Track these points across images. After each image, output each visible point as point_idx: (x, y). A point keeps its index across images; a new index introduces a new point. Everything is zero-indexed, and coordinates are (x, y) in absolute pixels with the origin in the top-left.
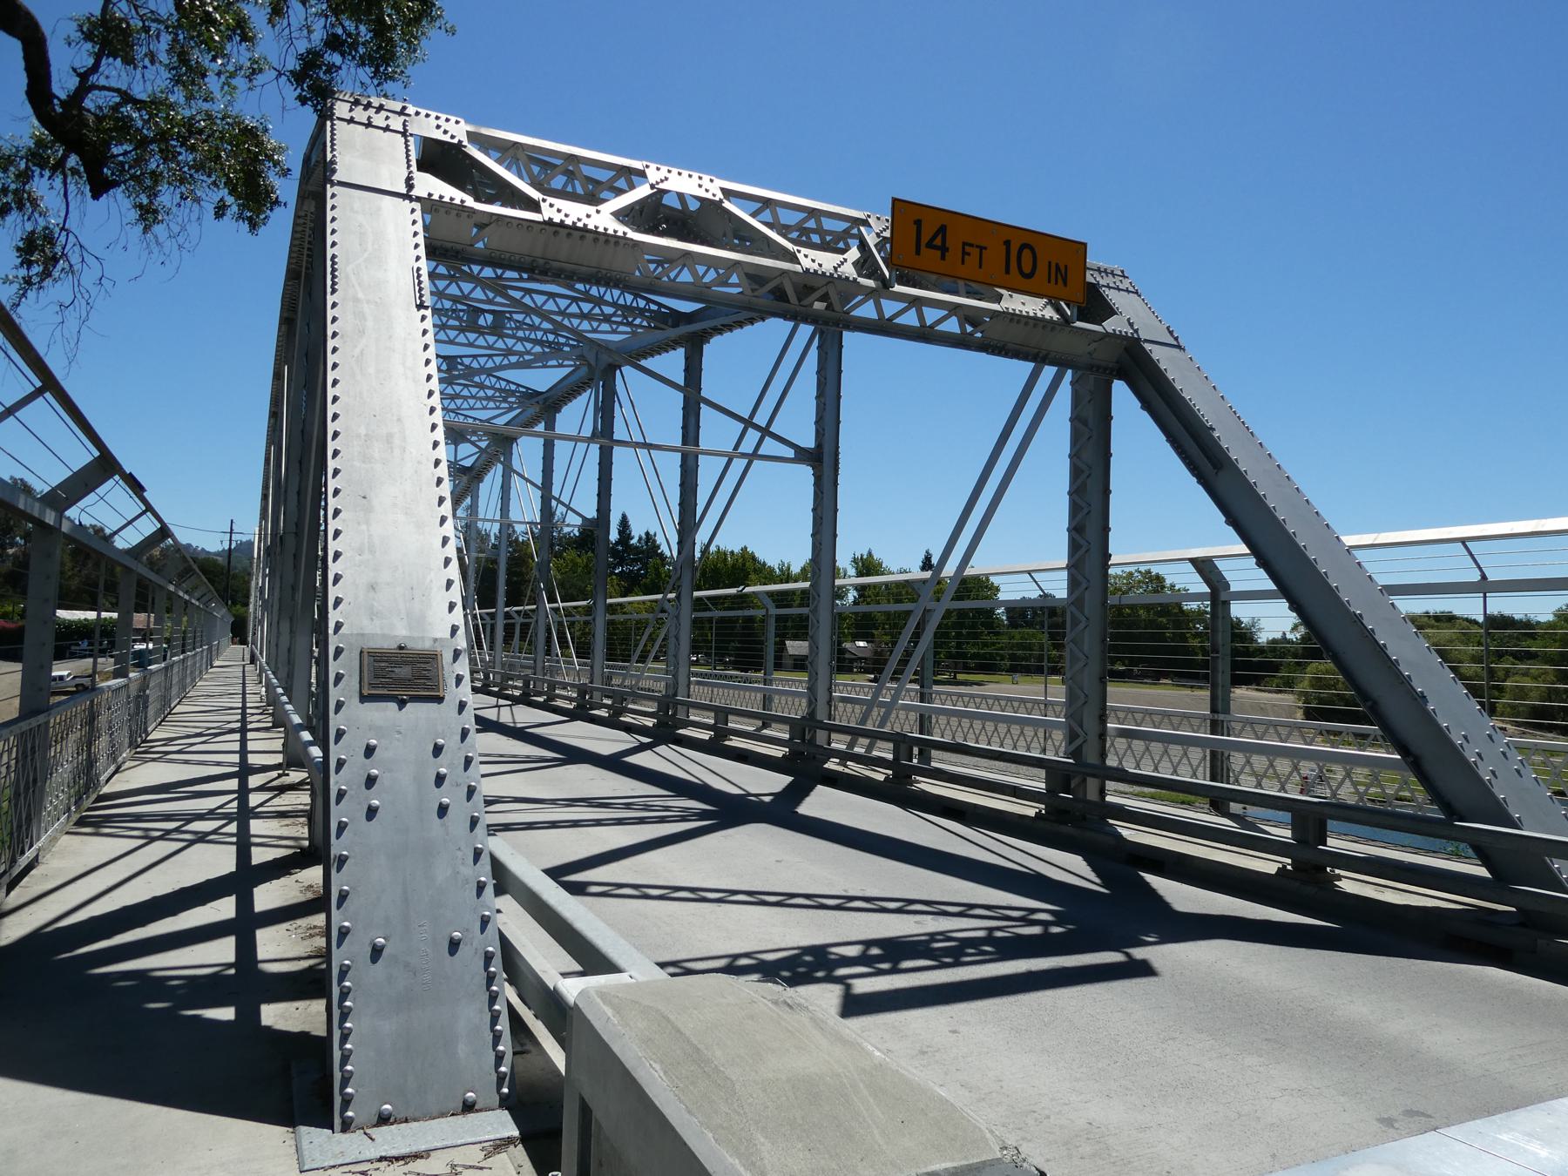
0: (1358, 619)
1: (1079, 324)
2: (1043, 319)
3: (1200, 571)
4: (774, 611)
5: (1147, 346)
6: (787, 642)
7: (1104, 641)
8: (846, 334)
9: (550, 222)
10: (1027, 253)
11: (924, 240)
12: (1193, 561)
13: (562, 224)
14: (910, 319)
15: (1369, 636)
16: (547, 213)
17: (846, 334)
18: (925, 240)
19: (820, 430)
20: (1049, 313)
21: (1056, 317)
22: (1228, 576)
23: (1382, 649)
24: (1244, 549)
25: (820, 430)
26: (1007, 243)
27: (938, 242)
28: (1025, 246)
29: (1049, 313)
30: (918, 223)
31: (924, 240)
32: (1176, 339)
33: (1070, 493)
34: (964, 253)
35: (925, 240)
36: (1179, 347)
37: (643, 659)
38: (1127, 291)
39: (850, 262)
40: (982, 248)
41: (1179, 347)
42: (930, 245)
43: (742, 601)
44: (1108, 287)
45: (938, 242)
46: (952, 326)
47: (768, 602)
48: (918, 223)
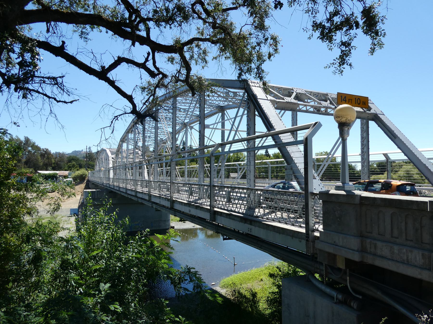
0: (425, 165)
1: (367, 112)
2: (361, 112)
3: (385, 156)
4: (270, 166)
5: (379, 115)
6: (230, 174)
7: (369, 170)
8: (298, 113)
9: (287, 102)
10: (359, 100)
11: (343, 99)
12: (383, 154)
13: (288, 102)
14: (304, 109)
15: (427, 168)
16: (286, 101)
17: (298, 113)
18: (343, 99)
19: (249, 128)
20: (361, 110)
21: (363, 111)
22: (390, 157)
23: (430, 170)
24: (401, 151)
25: (249, 128)
26: (356, 98)
27: (345, 99)
28: (358, 99)
29: (361, 110)
30: (341, 96)
31: (343, 99)
32: (267, 98)
33: (361, 142)
34: (349, 101)
35: (343, 99)
36: (384, 115)
37: (193, 177)
38: (258, 87)
39: (293, 98)
40: (352, 100)
41: (384, 115)
42: (343, 100)
43: (266, 163)
44: (253, 86)
45: (345, 99)
46: (312, 110)
47: (238, 165)
48: (341, 96)
